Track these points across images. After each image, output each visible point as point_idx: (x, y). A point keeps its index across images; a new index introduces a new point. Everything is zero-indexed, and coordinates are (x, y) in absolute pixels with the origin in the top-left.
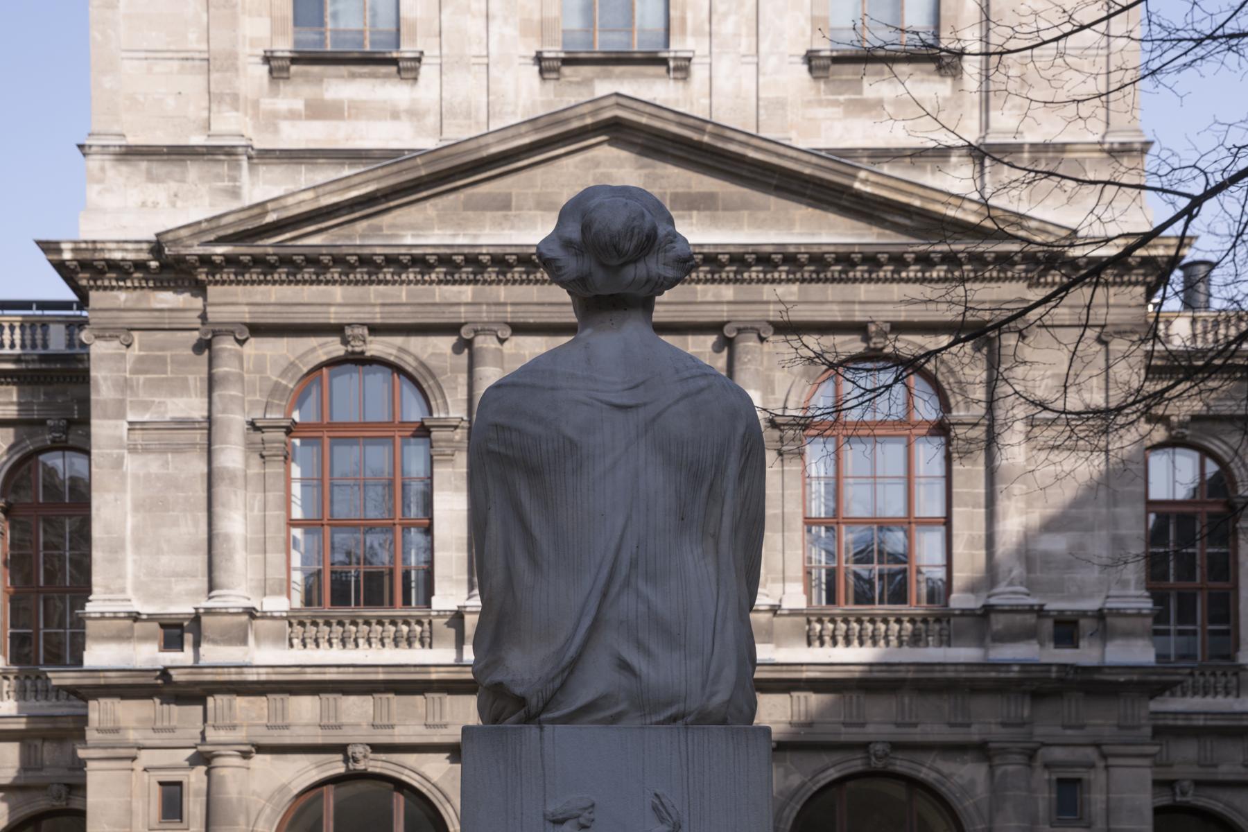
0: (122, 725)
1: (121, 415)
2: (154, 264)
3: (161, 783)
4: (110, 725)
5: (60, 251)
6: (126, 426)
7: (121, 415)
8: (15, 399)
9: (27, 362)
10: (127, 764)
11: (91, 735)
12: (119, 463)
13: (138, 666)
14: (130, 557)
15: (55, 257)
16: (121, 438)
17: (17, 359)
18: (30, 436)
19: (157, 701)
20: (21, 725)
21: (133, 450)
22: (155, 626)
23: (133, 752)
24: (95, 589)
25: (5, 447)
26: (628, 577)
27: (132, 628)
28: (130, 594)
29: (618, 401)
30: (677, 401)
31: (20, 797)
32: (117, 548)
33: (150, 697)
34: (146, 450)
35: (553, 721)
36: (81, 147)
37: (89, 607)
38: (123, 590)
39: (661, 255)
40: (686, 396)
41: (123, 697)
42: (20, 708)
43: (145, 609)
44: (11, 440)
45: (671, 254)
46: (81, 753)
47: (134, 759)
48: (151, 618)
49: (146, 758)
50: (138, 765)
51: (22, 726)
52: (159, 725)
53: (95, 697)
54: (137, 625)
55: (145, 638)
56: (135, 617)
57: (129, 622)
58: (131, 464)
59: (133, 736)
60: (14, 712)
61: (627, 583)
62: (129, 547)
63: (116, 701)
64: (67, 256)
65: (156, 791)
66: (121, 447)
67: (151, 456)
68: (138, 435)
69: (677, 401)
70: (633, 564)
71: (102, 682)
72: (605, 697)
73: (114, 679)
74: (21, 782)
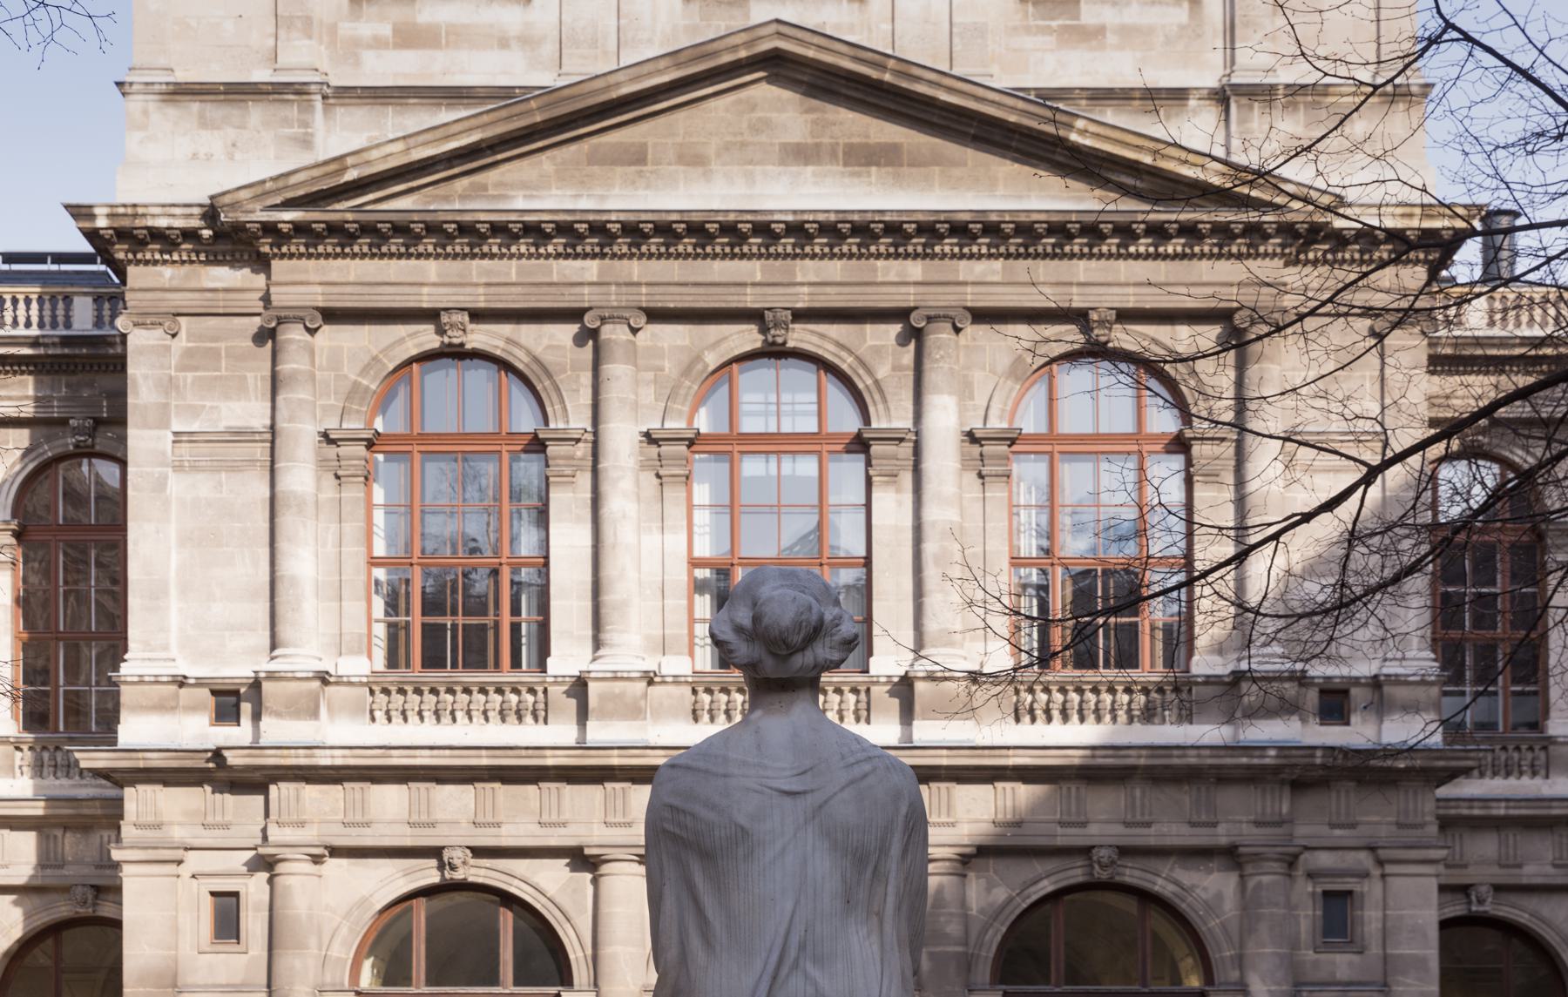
0: (165, 819)
1: (164, 423)
2: (206, 233)
3: (213, 894)
4: (150, 819)
5: (92, 217)
6: (171, 437)
7: (164, 423)
8: (31, 392)
9: (46, 345)
10: (172, 868)
11: (128, 831)
12: (161, 485)
13: (185, 747)
14: (174, 604)
15: (87, 225)
16: (164, 453)
17: (35, 342)
18: (48, 439)
19: (208, 789)
20: (38, 809)
21: (178, 467)
22: (206, 692)
23: (179, 854)
24: (131, 645)
25: (19, 453)
26: (797, 960)
27: (177, 696)
28: (174, 652)
29: (786, 788)
30: (843, 789)
31: (36, 901)
32: (158, 593)
33: (199, 784)
34: (195, 468)
36: (119, 84)
37: (126, 669)
38: (166, 648)
39: (827, 639)
40: (851, 782)
41: (166, 784)
42: (36, 787)
43: (193, 671)
44: (26, 444)
45: (836, 638)
46: (116, 855)
47: (180, 862)
48: (200, 683)
49: (194, 861)
50: (185, 871)
51: (40, 812)
52: (210, 819)
53: (132, 783)
54: (183, 691)
55: (193, 708)
56: (181, 682)
57: (174, 688)
58: (177, 485)
59: (179, 834)
60: (29, 793)
61: (796, 965)
62: (173, 591)
63: (158, 788)
64: (101, 223)
65: (208, 901)
66: (163, 464)
67: (200, 476)
68: (184, 449)
69: (843, 789)
70: (802, 947)
71: (141, 764)
73: (156, 761)
74: (38, 882)
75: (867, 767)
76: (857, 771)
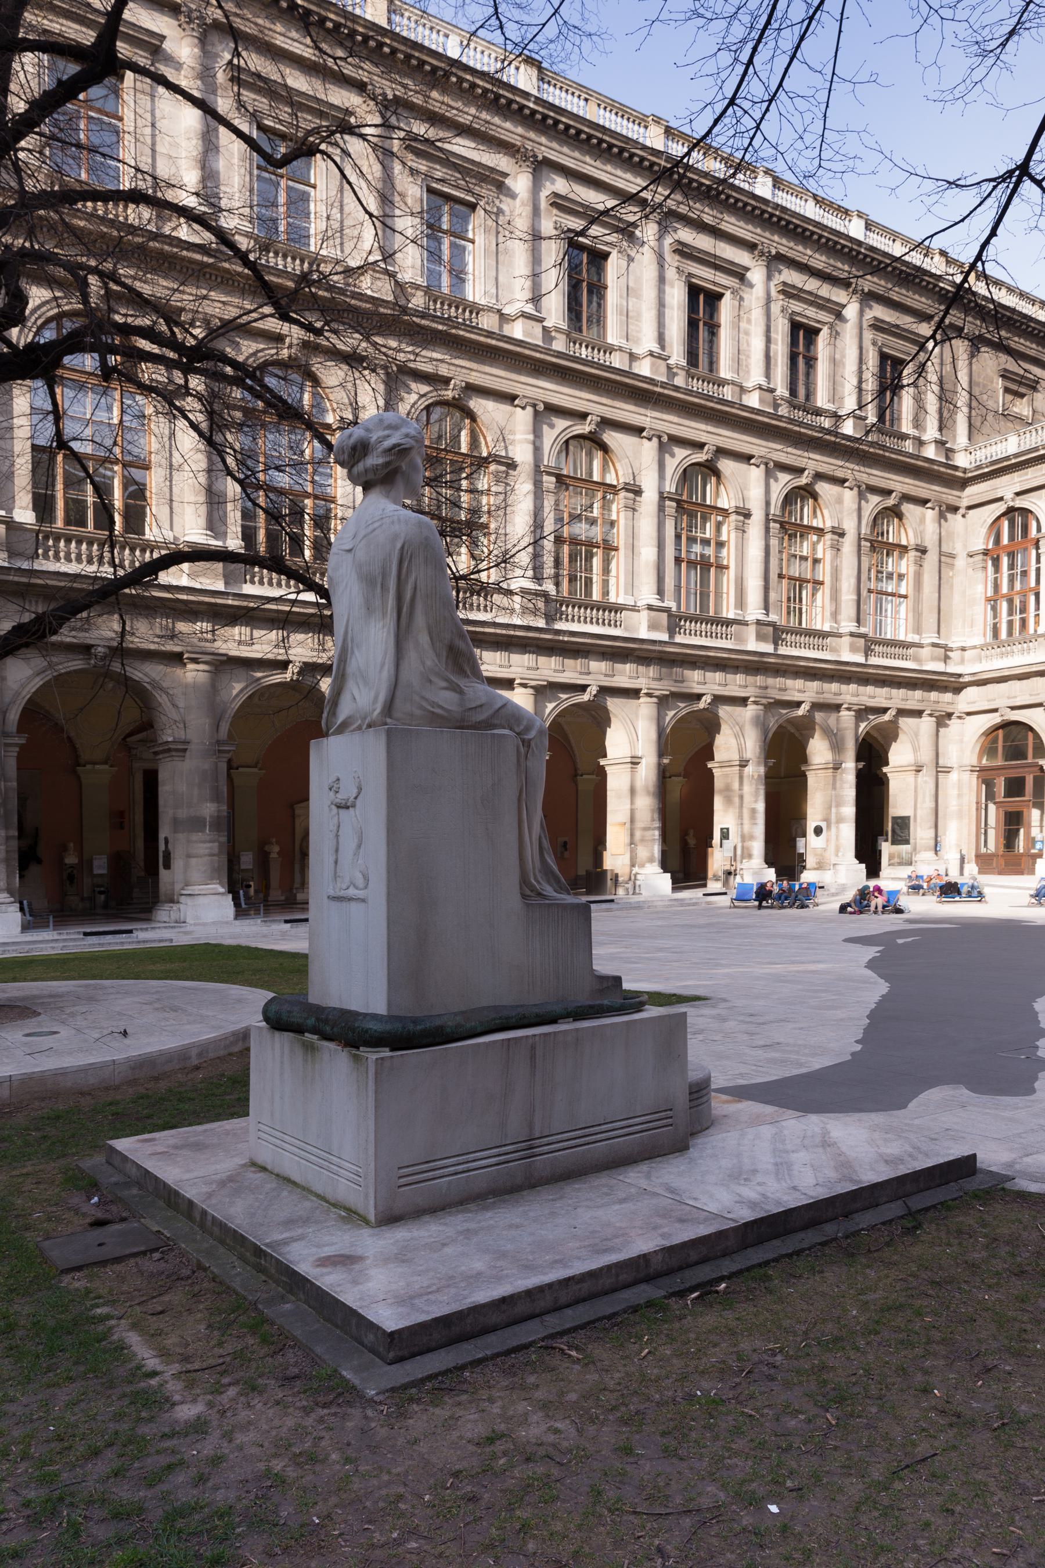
35: (333, 734)
72: (349, 717)
75: (376, 525)
76: (371, 528)
